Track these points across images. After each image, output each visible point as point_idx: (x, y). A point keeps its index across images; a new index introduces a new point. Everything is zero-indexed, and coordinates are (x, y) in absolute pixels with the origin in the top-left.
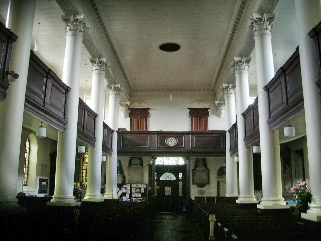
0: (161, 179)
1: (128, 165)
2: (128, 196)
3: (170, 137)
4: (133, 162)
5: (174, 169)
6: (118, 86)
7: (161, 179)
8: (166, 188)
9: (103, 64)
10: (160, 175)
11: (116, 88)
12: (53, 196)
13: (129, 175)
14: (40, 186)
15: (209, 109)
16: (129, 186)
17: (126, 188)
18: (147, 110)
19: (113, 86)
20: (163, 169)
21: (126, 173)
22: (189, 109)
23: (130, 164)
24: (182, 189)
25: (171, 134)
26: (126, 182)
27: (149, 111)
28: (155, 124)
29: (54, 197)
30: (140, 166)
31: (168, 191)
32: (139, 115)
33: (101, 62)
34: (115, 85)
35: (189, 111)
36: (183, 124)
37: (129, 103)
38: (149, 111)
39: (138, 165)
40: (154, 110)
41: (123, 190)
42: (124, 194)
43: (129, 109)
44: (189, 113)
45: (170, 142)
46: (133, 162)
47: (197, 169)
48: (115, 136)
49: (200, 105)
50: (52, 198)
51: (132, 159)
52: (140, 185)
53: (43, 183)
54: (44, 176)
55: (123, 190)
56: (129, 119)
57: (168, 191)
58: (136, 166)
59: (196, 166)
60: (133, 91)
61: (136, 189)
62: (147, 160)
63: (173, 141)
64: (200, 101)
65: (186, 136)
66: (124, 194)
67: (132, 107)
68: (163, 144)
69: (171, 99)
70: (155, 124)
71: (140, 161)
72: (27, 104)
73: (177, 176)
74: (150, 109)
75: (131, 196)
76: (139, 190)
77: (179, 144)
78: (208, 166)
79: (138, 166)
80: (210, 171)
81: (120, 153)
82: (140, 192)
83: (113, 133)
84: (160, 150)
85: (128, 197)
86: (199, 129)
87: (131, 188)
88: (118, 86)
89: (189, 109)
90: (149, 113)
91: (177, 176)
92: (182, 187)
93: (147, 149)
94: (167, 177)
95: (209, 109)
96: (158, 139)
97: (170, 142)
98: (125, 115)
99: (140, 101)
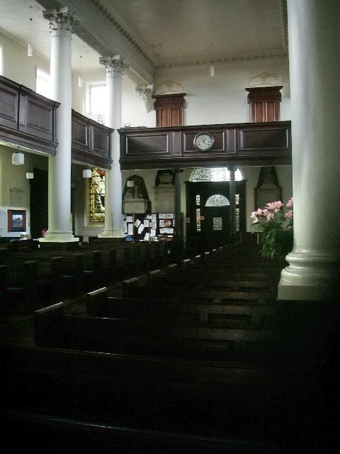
0: (208, 204)
1: (154, 185)
2: (153, 232)
3: (201, 134)
4: (162, 179)
5: (222, 188)
6: (117, 57)
7: (208, 204)
8: (214, 219)
9: (66, 18)
10: (204, 200)
11: (113, 61)
12: (289, 258)
13: (156, 200)
14: (10, 221)
15: (281, 87)
16: (155, 218)
17: (150, 221)
18: (182, 96)
19: (109, 59)
20: (208, 189)
21: (152, 197)
22: (247, 89)
23: (158, 182)
24: (196, 215)
25: (213, 128)
26: (153, 212)
27: (185, 98)
28: (193, 116)
29: (297, 263)
30: (172, 185)
31: (218, 223)
32: (168, 104)
33: (60, 15)
34: (112, 57)
35: (248, 93)
36: (240, 113)
37: (151, 87)
38: (185, 98)
39: (168, 183)
40: (192, 95)
41: (146, 224)
42: (147, 230)
43: (153, 97)
44: (249, 96)
45: (202, 143)
46: (162, 179)
47: (261, 187)
48: (116, 139)
49: (266, 82)
50: (286, 264)
51: (160, 173)
52: (165, 215)
53: (15, 217)
54: (21, 206)
55: (146, 224)
56: (154, 113)
57: (218, 223)
58: (167, 185)
59: (260, 183)
60: (158, 67)
61: (166, 220)
62: (181, 178)
63: (207, 142)
64: (265, 76)
65: (228, 131)
66: (147, 230)
67: (159, 93)
68: (191, 146)
69: (212, 74)
70: (193, 116)
71: (171, 177)
72: (74, 118)
73: (232, 200)
74: (185, 94)
75: (158, 232)
76: (169, 223)
77: (216, 146)
78: (280, 183)
79: (170, 185)
80: (283, 190)
81: (125, 164)
82: (171, 227)
83: (112, 134)
84: (187, 156)
85: (154, 234)
86: (265, 120)
87: (158, 220)
88: (117, 57)
89: (247, 89)
90: (184, 100)
91: (232, 200)
92: (240, 216)
93: (167, 157)
94: (217, 200)
95: (281, 87)
96: (182, 139)
97: (202, 143)
98: (147, 106)
99: (170, 83)
